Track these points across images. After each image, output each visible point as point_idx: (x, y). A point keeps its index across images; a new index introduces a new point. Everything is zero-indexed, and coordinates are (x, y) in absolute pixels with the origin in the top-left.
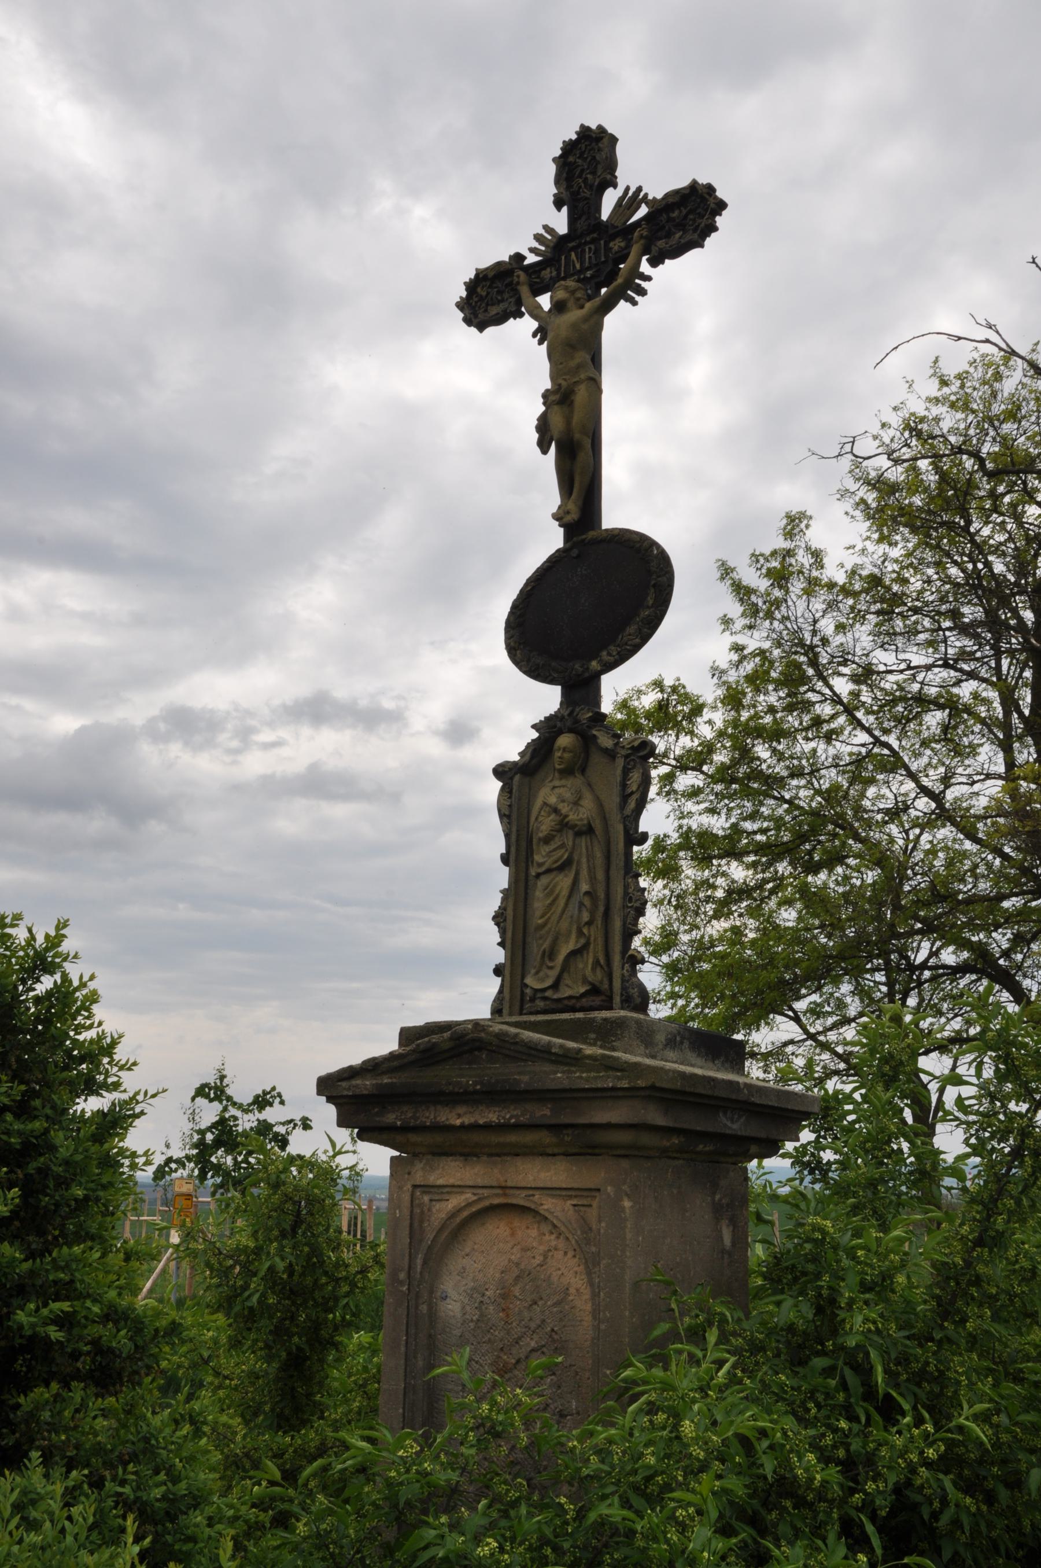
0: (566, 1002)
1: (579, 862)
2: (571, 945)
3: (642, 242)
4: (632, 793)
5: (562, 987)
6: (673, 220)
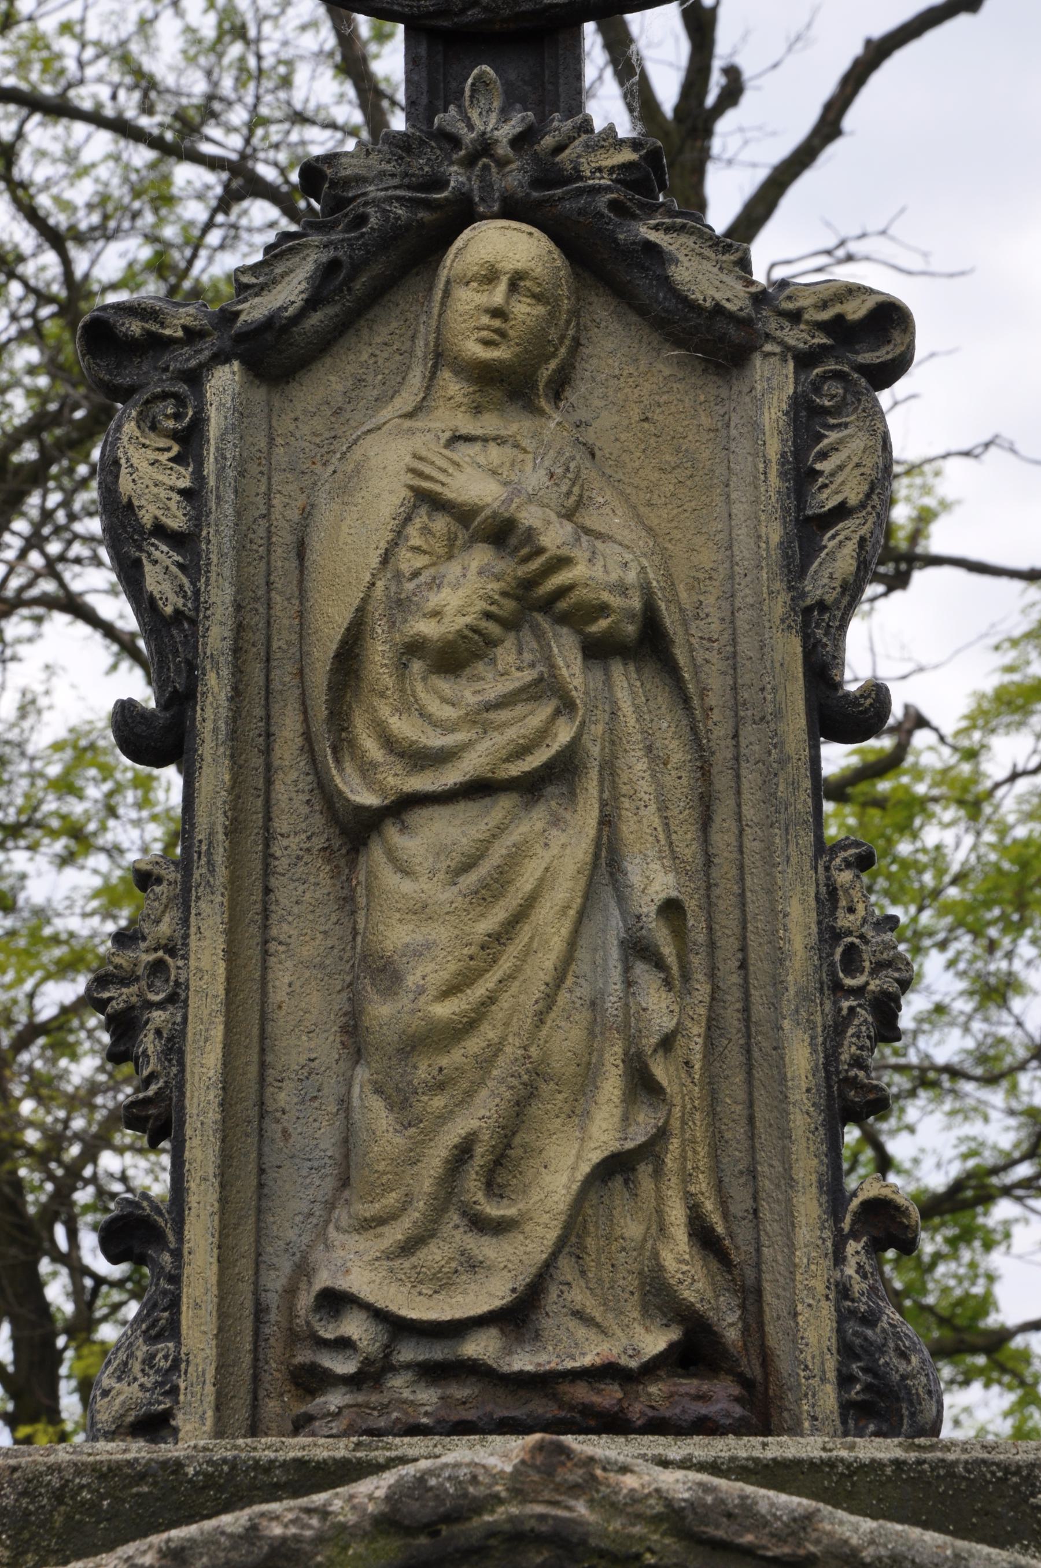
0: (581, 1393)
1: (609, 769)
2: (605, 1132)
4: (842, 511)
5: (553, 1320)
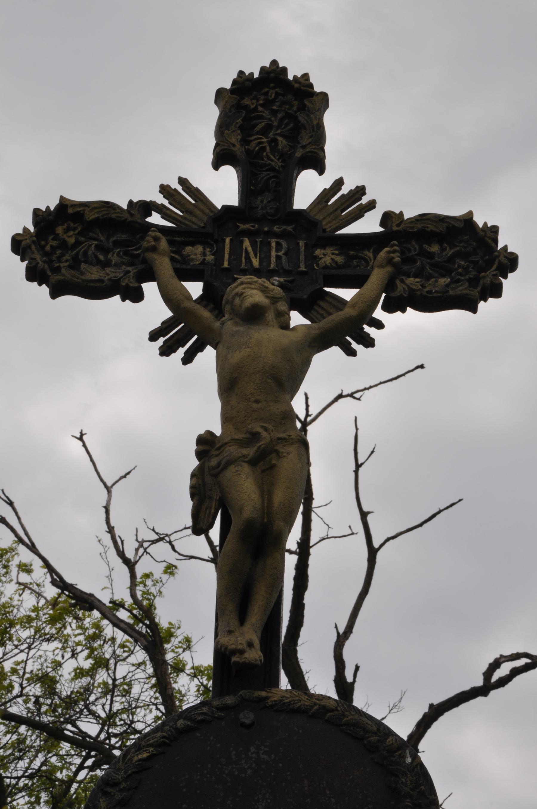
3: (389, 269)
6: (431, 256)
